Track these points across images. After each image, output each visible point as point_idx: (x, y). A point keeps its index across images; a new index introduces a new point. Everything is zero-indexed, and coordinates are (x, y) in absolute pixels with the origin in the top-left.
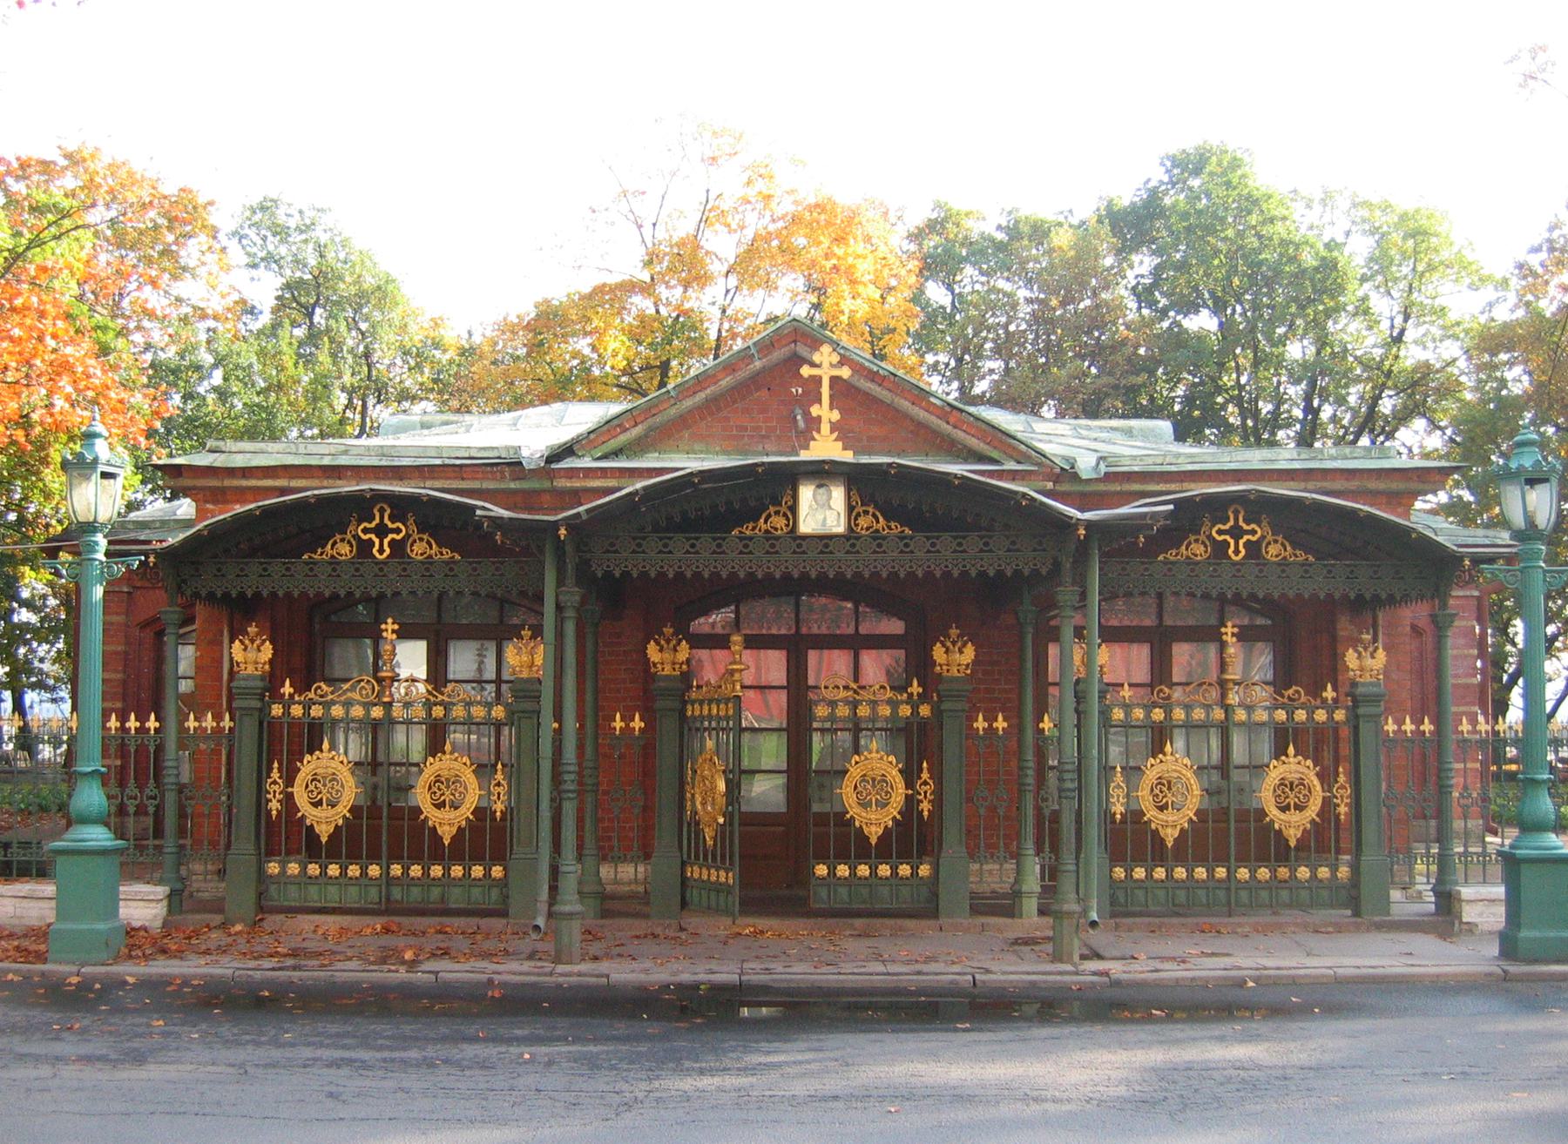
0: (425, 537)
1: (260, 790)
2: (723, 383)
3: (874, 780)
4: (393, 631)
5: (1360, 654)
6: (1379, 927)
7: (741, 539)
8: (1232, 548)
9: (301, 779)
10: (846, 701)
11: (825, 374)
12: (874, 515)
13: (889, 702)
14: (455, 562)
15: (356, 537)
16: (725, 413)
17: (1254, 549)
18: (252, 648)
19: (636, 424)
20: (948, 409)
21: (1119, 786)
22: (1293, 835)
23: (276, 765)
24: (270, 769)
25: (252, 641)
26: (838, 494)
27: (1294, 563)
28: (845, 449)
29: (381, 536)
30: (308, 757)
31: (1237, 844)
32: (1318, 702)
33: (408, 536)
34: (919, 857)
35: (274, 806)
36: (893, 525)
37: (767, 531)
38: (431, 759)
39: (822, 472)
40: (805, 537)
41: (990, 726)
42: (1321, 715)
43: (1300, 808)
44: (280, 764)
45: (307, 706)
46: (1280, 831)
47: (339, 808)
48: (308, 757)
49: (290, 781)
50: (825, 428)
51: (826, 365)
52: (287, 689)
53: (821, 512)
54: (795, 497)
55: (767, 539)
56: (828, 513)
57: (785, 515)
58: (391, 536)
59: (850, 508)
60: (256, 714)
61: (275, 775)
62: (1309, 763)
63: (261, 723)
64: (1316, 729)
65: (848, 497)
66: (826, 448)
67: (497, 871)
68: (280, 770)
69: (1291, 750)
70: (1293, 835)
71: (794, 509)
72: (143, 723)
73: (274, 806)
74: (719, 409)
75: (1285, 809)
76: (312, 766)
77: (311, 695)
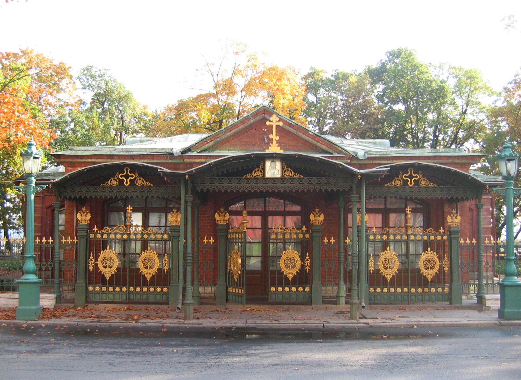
0: (141, 178)
1: (86, 262)
2: (240, 127)
3: (290, 259)
4: (131, 210)
5: (452, 217)
6: (458, 308)
7: (246, 179)
8: (409, 182)
9: (100, 259)
10: (281, 233)
11: (274, 124)
12: (290, 171)
13: (295, 233)
14: (151, 187)
15: (118, 178)
16: (241, 137)
17: (417, 182)
18: (84, 215)
19: (211, 141)
20: (315, 136)
21: (372, 261)
22: (430, 277)
23: (92, 254)
24: (90, 256)
25: (84, 213)
26: (278, 164)
27: (430, 187)
28: (281, 149)
29: (127, 178)
30: (102, 252)
31: (411, 280)
32: (438, 233)
33: (136, 178)
34: (305, 285)
35: (91, 268)
36: (297, 174)
37: (255, 177)
38: (143, 252)
39: (273, 157)
40: (267, 178)
41: (329, 241)
42: (439, 238)
43: (432, 268)
44: (93, 254)
45: (102, 235)
46: (425, 276)
47: (113, 268)
48: (102, 252)
49: (96, 260)
50: (274, 142)
51: (274, 121)
52: (95, 229)
53: (273, 170)
54: (264, 165)
55: (255, 179)
56: (275, 170)
57: (261, 171)
58: (130, 178)
59: (283, 169)
60: (85, 237)
61: (91, 257)
62: (435, 253)
63: (87, 240)
64: (437, 242)
65: (282, 165)
66: (274, 149)
67: (165, 289)
68: (93, 256)
69: (429, 249)
70: (430, 277)
71: (264, 169)
72: (47, 240)
73: (91, 268)
74: (239, 136)
75: (427, 269)
76: (104, 254)
77: (103, 231)
